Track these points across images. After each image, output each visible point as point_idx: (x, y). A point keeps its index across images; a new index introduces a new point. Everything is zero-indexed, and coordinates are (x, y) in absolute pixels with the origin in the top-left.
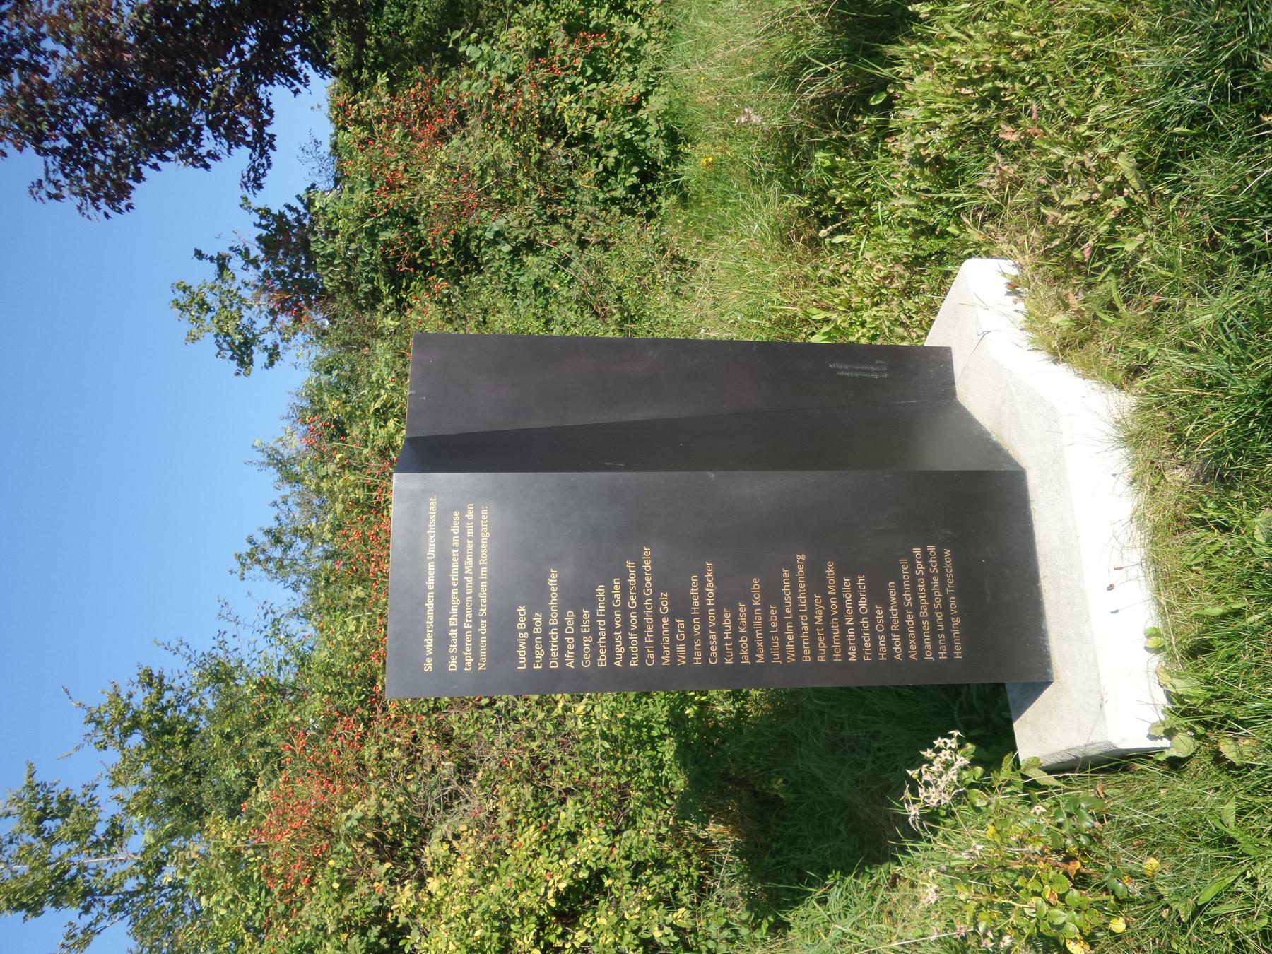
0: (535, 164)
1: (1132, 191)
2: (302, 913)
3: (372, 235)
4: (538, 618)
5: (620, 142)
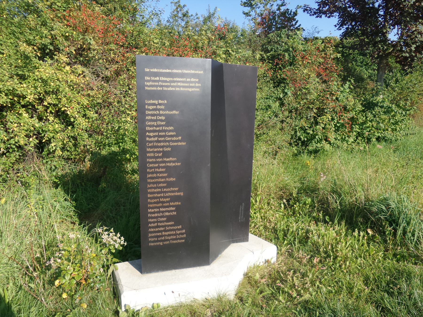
2: (58, 23)
3: (287, 50)
4: (162, 107)
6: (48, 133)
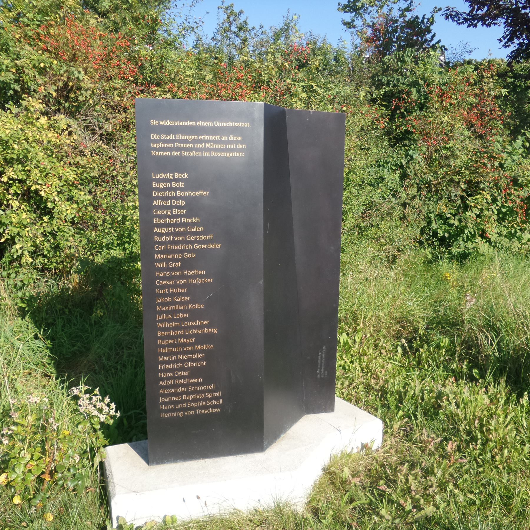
0: (452, 178)
1: (415, 514)
3: (415, 84)
4: (181, 185)
5: (463, 227)
6: (10, 227)
